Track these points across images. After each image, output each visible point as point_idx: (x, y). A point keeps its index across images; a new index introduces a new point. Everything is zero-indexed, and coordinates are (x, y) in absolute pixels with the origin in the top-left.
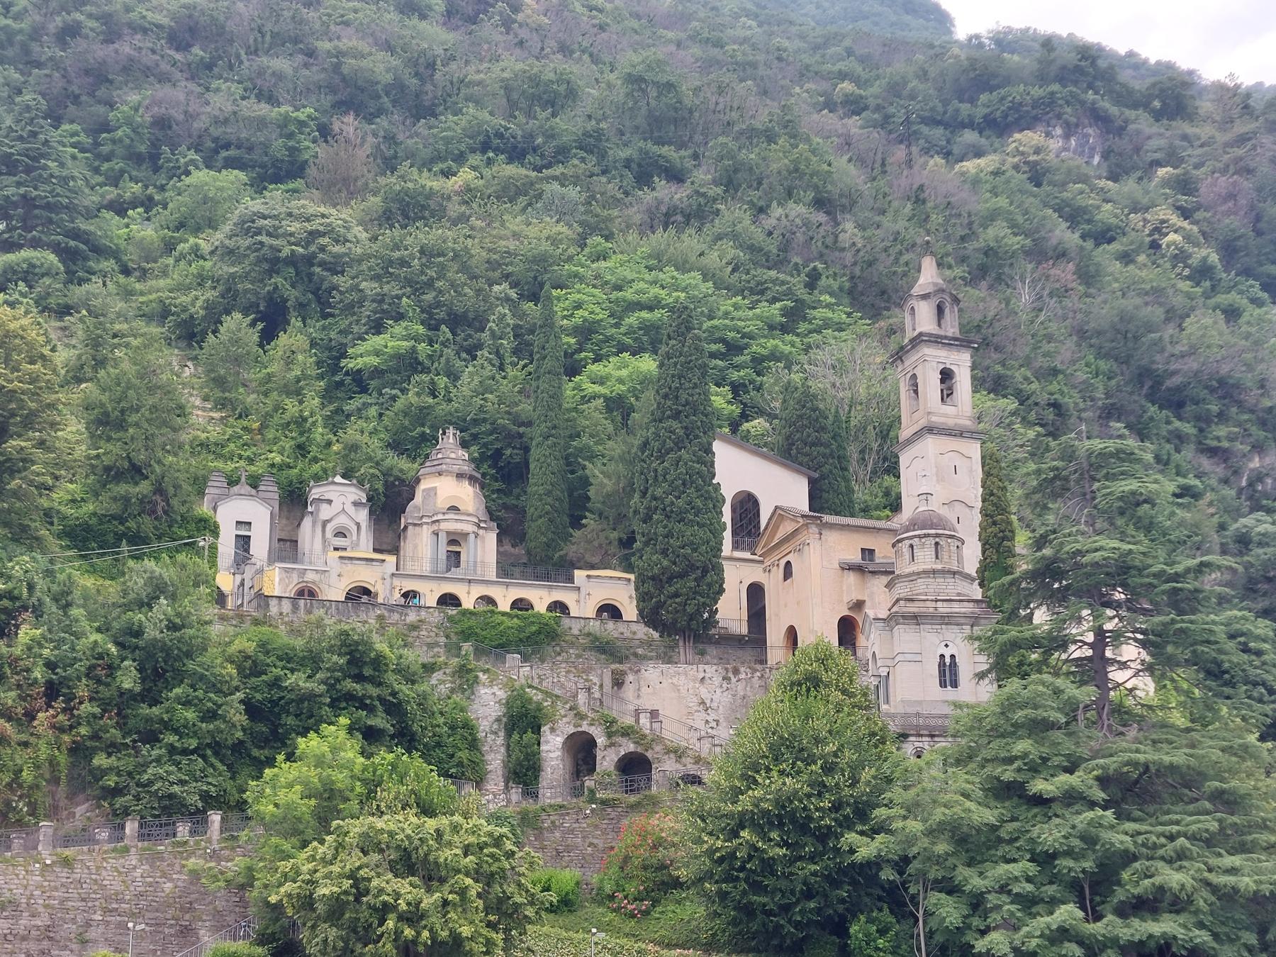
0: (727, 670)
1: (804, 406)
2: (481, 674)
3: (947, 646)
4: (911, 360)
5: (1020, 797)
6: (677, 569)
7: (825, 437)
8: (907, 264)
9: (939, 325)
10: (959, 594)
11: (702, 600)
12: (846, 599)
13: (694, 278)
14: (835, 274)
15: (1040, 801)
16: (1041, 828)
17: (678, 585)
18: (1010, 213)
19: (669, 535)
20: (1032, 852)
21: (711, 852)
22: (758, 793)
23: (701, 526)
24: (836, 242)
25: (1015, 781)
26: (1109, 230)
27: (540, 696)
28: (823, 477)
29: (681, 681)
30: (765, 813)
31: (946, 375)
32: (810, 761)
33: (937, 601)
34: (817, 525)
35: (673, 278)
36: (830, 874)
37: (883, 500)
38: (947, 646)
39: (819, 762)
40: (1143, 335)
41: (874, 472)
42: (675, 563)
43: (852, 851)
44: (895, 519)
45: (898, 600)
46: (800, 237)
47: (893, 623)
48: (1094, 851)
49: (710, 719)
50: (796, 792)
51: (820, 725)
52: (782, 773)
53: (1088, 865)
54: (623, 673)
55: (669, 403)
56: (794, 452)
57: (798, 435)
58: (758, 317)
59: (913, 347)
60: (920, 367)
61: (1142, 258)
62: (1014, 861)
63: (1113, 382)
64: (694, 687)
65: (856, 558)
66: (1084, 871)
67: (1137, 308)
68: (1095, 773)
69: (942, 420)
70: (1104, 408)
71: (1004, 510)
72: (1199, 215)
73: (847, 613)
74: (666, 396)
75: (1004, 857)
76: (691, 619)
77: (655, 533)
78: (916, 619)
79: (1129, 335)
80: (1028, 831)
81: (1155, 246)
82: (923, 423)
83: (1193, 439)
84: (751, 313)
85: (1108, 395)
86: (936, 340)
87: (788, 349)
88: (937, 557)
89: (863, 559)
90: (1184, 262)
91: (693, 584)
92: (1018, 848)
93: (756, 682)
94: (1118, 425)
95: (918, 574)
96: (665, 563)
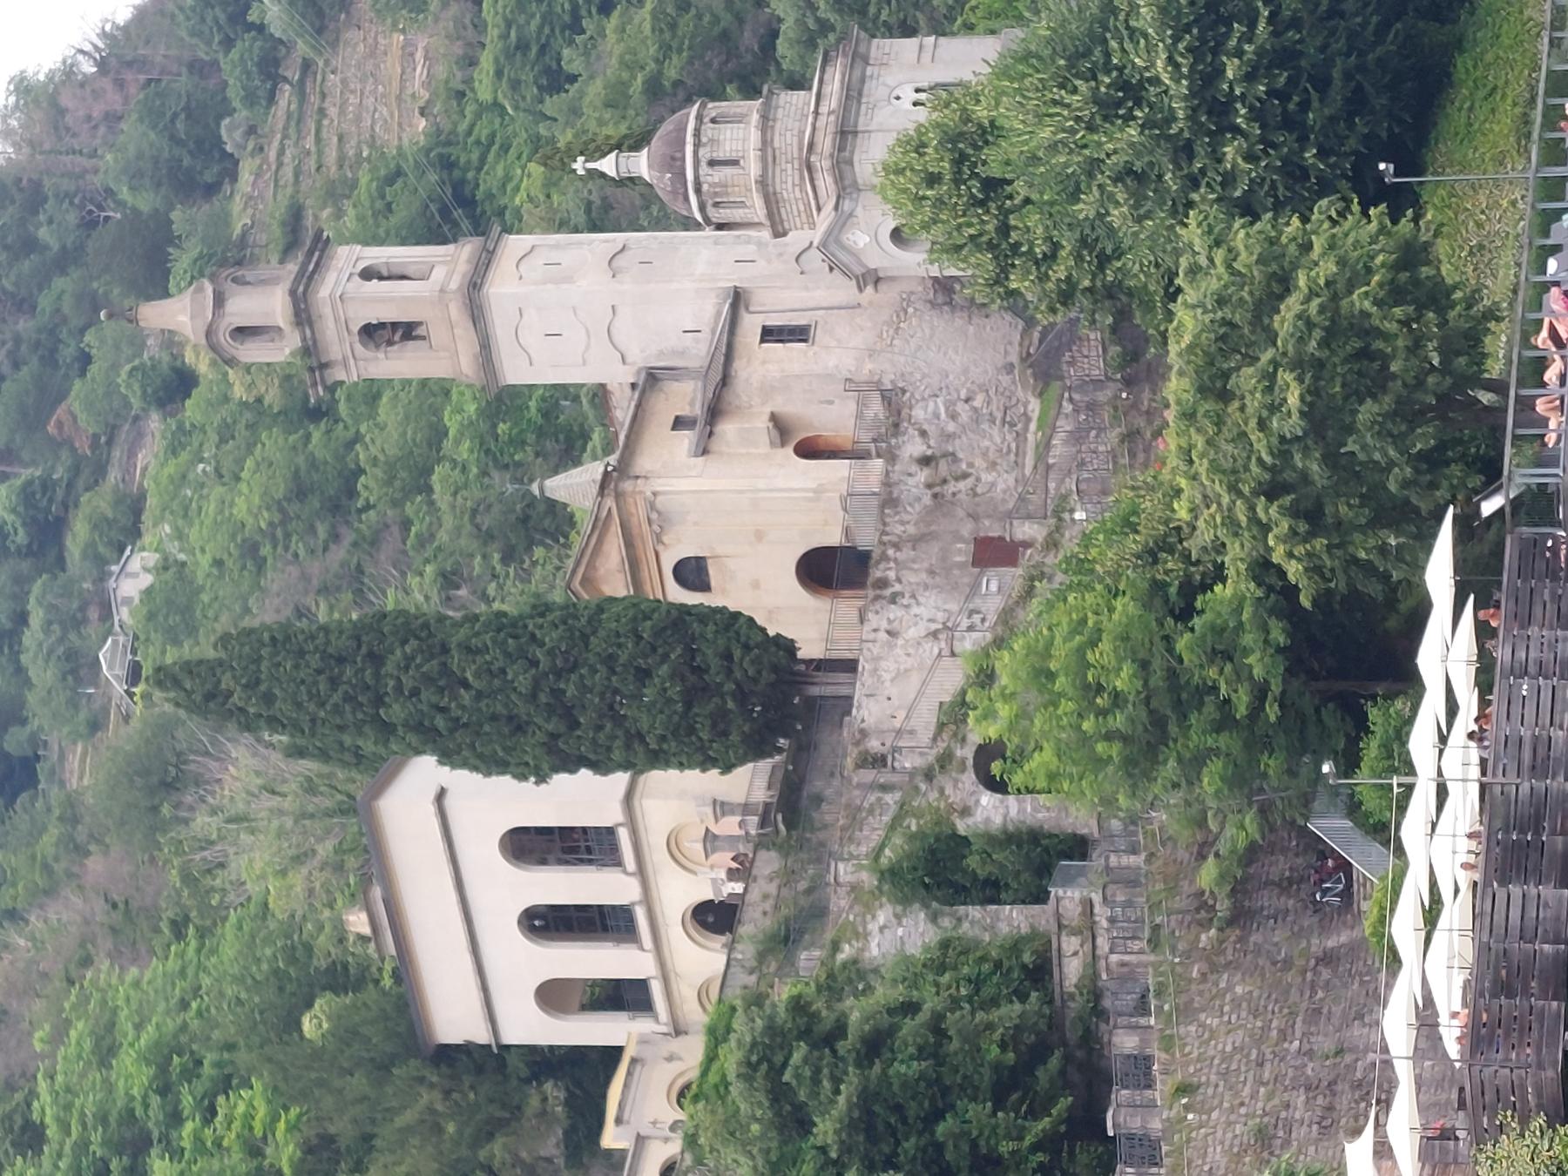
0: (877, 598)
2: (841, 957)
12: (764, 447)
19: (610, 660)
27: (898, 840)
29: (888, 667)
33: (816, 113)
34: (620, 479)
42: (665, 657)
55: (349, 672)
73: (790, 450)
82: (456, 311)
93: (905, 554)
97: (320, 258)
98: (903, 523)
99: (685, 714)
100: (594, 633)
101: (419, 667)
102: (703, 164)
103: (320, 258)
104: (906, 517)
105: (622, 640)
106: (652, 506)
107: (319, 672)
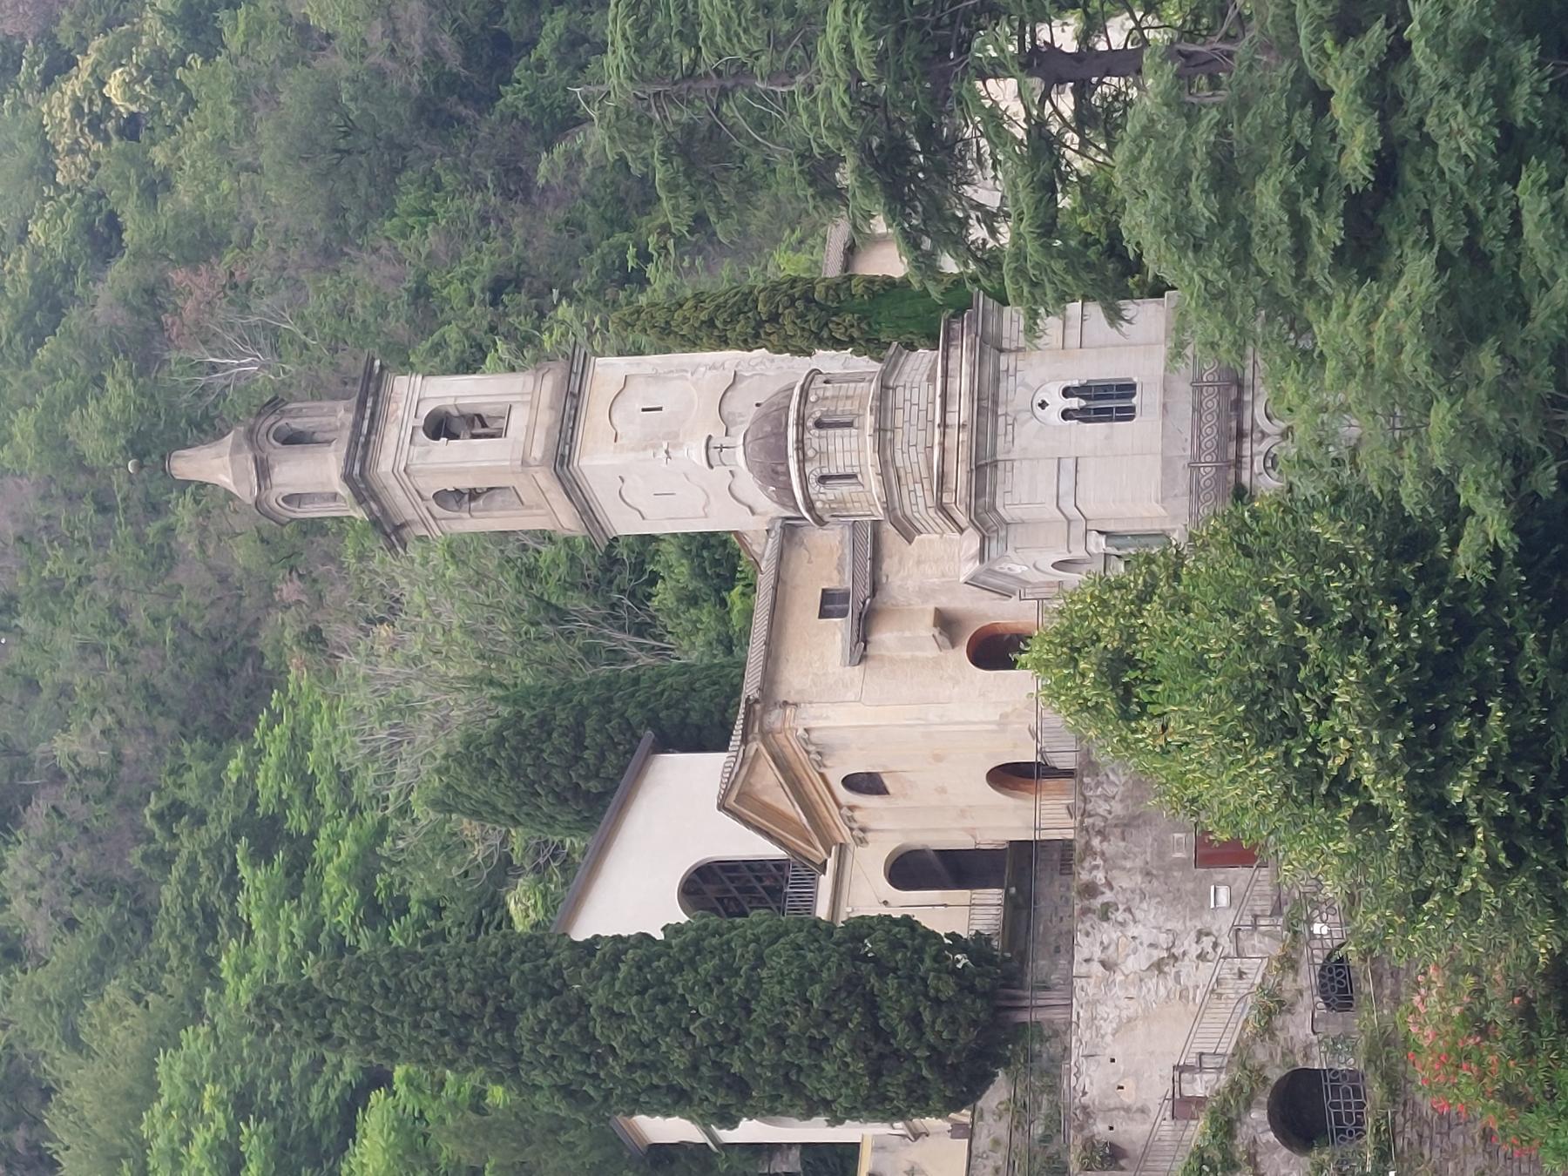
0: (1086, 911)
1: (492, 763)
3: (1043, 405)
4: (403, 504)
5: (1377, 210)
6: (857, 1018)
7: (562, 716)
8: (157, 620)
9: (329, 442)
10: (931, 379)
11: (928, 962)
12: (931, 651)
13: (170, 1071)
14: (172, 772)
15: (1386, 165)
16: (1447, 157)
17: (892, 1017)
18: (49, 408)
19: (778, 1035)
20: (1498, 179)
21: (1496, 875)
22: (1368, 764)
23: (760, 961)
24: (98, 773)
25: (1345, 213)
26: (89, 229)
28: (653, 722)
30: (1411, 751)
31: (441, 426)
32: (1296, 653)
33: (944, 425)
34: (766, 710)
35: (167, 1114)
36: (1545, 614)
37: (707, 607)
38: (1043, 405)
39: (1301, 631)
40: (345, 115)
41: (641, 630)
42: (843, 1024)
43: (1496, 555)
44: (756, 548)
45: (942, 508)
46: (81, 859)
47: (991, 519)
48: (1497, 44)
49: (1194, 951)
50: (1365, 682)
51: (1219, 636)
52: (1322, 715)
53: (1526, 55)
54: (1090, 1145)
55: (477, 1035)
56: (594, 786)
57: (557, 775)
58: (272, 915)
59: (375, 498)
60: (421, 483)
61: (159, 155)
62: (1516, 215)
63: (447, 178)
64: (1125, 988)
65: (839, 631)
66: (1539, 65)
67: (281, 127)
68: (1329, 45)
69: (540, 437)
70: (508, 196)
71: (747, 299)
72: (66, 36)
73: (962, 653)
74: (462, 1044)
75: (1507, 238)
76: (972, 989)
77: (774, 1068)
78: (984, 467)
79: (342, 144)
80: (1453, 189)
81: (131, 128)
82: (544, 478)
83: (577, 16)
84: (260, 934)
85: (480, 186)
86: (362, 446)
87: (347, 846)
88: (849, 425)
89: (843, 614)
90: (173, 65)
91: (892, 982)
92: (1489, 210)
93: (1113, 846)
94: (543, 168)
95: (884, 463)
96: (842, 1044)
97: (375, 403)
98: (1107, 799)
99: (874, 1085)
100: (756, 997)
101: (556, 1033)
102: (813, 480)
103: (375, 403)
104: (1111, 791)
105: (789, 1008)
106: (807, 742)
107: (443, 1033)
